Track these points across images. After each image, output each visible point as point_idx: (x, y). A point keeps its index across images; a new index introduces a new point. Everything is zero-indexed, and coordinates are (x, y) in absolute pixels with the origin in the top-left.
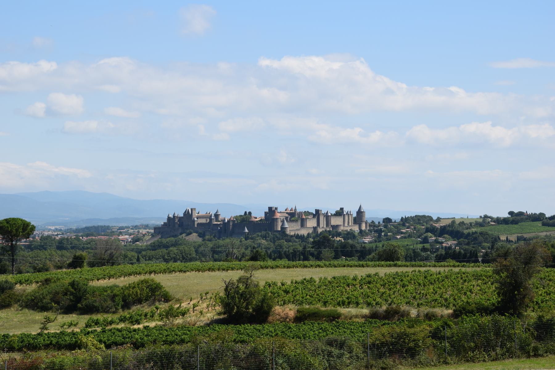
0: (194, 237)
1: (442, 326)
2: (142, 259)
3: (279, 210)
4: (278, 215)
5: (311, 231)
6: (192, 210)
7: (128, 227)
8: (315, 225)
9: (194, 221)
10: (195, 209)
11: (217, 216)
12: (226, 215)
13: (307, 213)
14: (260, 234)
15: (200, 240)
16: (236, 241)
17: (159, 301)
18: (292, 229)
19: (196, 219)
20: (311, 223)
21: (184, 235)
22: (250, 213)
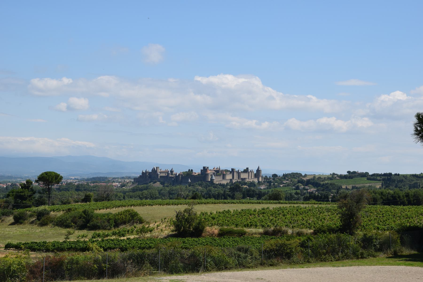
0: (158, 185)
1: (307, 240)
2: (126, 197)
3: (209, 169)
4: (209, 172)
5: (228, 182)
6: (157, 168)
7: (118, 178)
8: (231, 178)
9: (158, 175)
10: (159, 167)
11: (172, 172)
12: (178, 171)
13: (227, 171)
14: (198, 183)
15: (161, 186)
16: (183, 187)
17: (137, 223)
18: (217, 180)
19: (159, 173)
20: (229, 177)
21: (152, 183)
22: (192, 170)
